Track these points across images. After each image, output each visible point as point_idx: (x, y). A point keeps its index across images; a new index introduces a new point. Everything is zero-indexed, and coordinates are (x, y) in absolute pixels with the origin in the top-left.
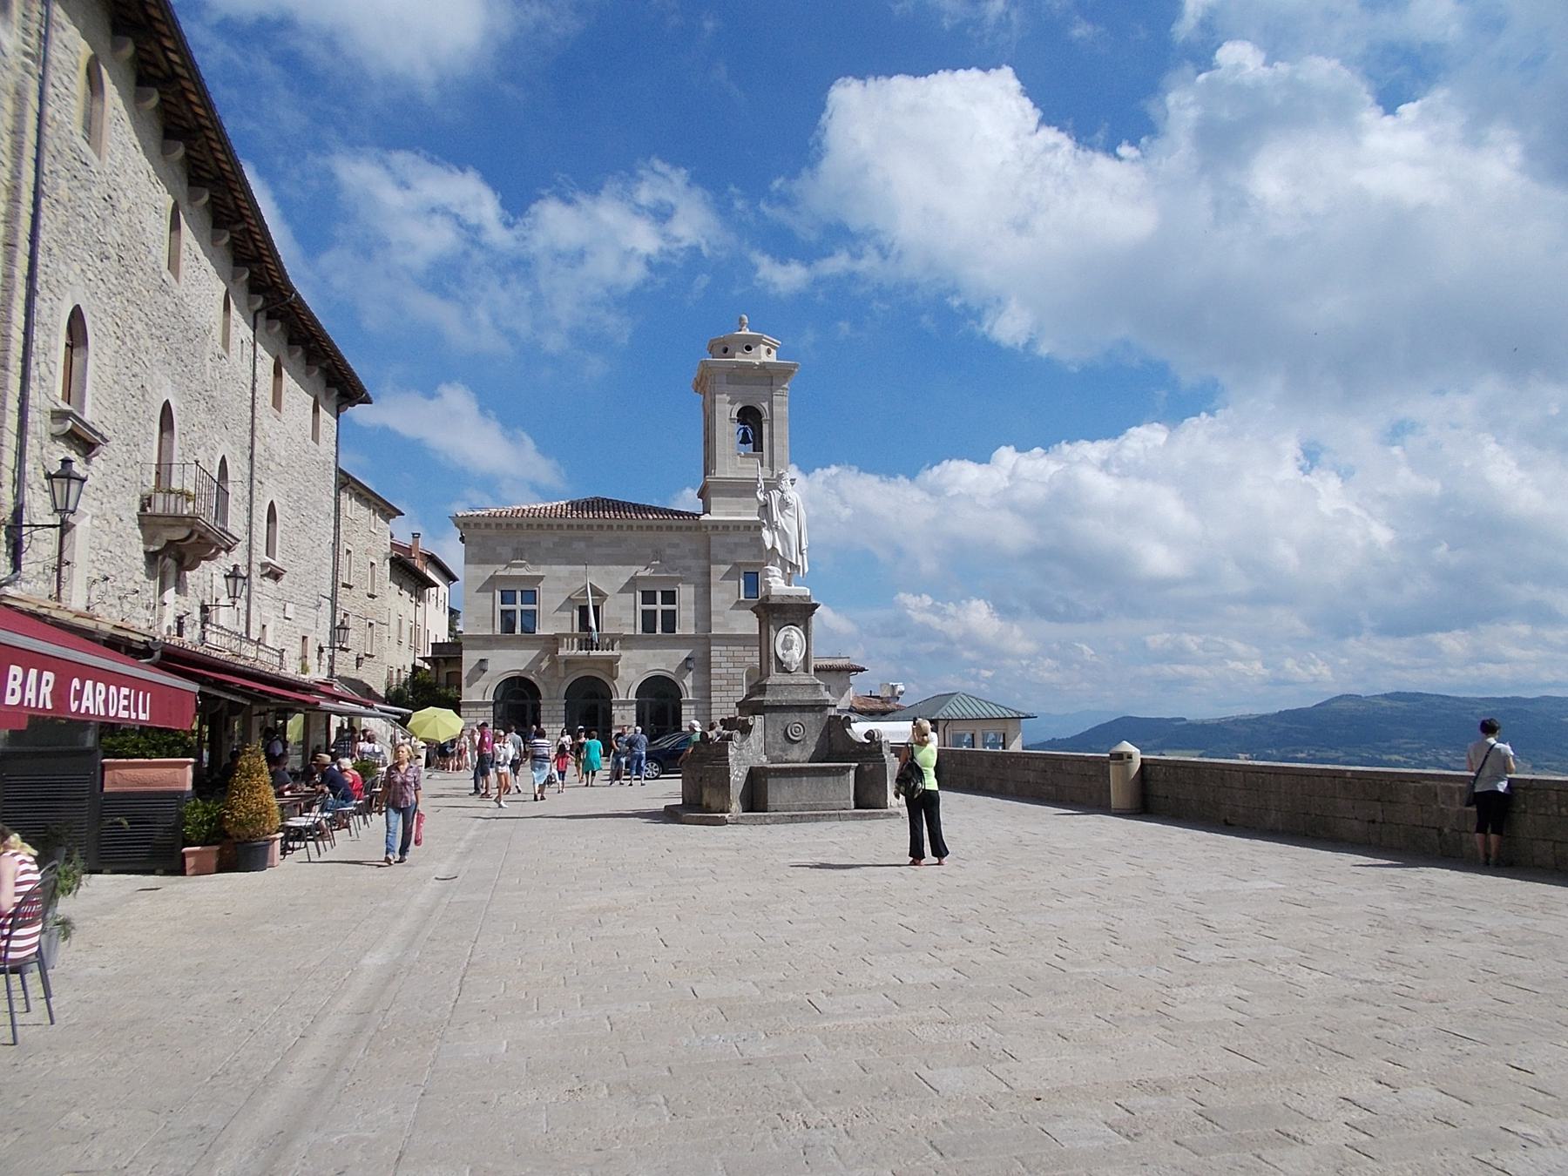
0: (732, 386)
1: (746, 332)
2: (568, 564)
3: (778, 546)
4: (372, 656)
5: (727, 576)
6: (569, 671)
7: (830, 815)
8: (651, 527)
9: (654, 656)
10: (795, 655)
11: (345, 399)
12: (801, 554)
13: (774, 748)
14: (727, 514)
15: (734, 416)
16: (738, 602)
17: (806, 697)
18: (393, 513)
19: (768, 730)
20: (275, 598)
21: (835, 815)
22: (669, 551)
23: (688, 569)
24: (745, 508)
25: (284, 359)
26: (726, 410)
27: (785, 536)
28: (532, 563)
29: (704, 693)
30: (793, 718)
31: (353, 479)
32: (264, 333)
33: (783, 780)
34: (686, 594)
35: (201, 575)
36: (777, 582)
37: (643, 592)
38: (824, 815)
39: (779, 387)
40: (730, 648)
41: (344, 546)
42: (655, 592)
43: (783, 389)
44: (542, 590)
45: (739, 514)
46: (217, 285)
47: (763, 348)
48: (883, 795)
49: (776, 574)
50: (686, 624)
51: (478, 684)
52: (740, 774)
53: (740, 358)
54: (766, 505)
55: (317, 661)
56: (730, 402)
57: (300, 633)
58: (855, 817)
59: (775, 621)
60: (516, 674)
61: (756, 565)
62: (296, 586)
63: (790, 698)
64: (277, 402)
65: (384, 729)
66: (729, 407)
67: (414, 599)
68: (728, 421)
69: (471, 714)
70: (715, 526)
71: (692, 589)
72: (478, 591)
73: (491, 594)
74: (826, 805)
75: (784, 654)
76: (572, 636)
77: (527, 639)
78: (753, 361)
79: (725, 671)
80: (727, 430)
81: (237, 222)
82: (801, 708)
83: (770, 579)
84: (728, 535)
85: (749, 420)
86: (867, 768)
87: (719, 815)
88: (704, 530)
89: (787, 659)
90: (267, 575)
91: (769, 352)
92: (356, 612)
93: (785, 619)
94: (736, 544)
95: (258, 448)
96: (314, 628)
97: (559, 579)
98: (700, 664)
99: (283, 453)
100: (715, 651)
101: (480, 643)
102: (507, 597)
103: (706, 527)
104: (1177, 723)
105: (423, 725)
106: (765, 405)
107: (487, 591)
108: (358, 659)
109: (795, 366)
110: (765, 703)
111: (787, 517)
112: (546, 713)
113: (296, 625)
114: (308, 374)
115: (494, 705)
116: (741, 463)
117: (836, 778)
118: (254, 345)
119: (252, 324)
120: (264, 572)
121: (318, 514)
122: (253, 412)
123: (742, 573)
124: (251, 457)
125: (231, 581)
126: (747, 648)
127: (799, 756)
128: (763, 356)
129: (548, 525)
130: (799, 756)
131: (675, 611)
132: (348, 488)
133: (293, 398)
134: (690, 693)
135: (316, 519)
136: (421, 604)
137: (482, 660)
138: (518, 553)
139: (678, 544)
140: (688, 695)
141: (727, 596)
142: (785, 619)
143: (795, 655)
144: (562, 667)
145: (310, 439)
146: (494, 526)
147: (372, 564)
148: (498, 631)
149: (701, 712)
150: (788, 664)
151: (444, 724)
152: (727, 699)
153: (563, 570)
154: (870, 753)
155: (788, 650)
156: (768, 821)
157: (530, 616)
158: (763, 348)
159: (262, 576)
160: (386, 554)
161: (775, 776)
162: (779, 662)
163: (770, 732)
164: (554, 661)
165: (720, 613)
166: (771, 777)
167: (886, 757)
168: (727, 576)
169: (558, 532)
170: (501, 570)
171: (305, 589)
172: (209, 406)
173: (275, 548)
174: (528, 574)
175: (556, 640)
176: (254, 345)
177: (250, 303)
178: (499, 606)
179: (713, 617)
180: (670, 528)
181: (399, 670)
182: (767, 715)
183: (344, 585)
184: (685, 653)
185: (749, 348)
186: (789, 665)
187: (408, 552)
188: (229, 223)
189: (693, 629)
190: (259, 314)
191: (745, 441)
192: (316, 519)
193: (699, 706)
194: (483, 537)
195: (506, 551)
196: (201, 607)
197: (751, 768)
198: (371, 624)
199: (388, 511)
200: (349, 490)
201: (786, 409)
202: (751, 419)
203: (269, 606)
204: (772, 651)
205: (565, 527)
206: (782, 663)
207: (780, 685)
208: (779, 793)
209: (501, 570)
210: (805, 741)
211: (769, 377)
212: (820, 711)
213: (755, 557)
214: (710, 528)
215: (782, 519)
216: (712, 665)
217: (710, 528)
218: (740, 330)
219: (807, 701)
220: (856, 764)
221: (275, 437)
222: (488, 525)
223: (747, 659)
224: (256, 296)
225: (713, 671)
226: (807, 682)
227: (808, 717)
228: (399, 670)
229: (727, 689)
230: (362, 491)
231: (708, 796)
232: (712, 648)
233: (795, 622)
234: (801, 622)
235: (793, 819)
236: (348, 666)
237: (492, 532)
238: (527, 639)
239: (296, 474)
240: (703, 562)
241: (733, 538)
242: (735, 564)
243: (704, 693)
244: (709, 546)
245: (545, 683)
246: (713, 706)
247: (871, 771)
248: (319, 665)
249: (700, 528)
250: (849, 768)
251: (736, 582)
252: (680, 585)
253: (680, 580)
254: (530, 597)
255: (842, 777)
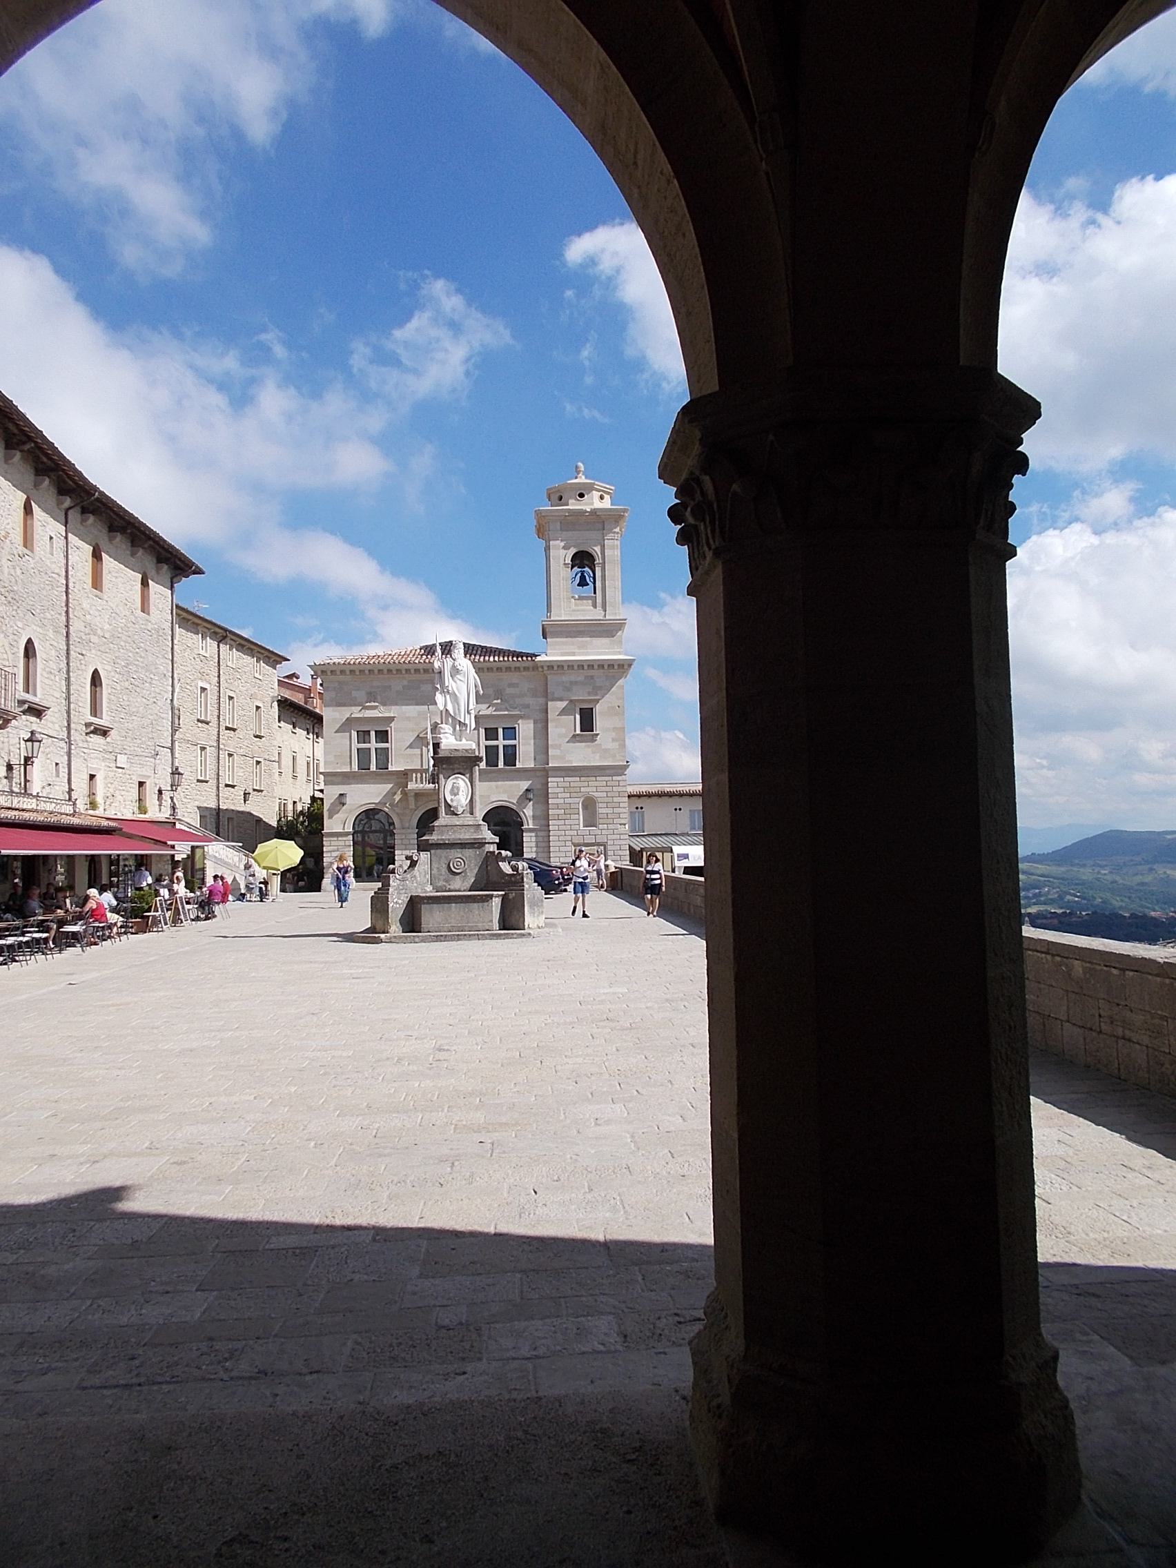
0: (564, 533)
1: (582, 479)
2: (417, 704)
3: (450, 708)
4: (262, 791)
5: (564, 712)
6: (420, 803)
7: (470, 935)
8: (492, 669)
9: (497, 787)
10: (462, 800)
11: (178, 572)
12: (469, 713)
13: (439, 879)
14: (562, 655)
15: (569, 561)
16: (574, 736)
17: (466, 836)
18: (278, 659)
19: (433, 864)
20: (105, 751)
21: (475, 935)
22: (509, 691)
23: (528, 706)
24: (579, 648)
25: (104, 543)
26: (562, 554)
27: (455, 699)
28: (384, 704)
29: (543, 822)
30: (456, 853)
31: (231, 632)
32: (79, 526)
33: (435, 905)
34: (526, 729)
35: (6, 740)
36: (447, 738)
37: (485, 729)
38: (465, 935)
39: (611, 531)
40: (566, 779)
41: (226, 693)
42: (497, 729)
43: (615, 533)
44: (394, 731)
45: (574, 654)
46: (14, 496)
47: (596, 494)
48: (522, 919)
49: (447, 731)
50: (526, 759)
51: (339, 816)
52: (400, 901)
53: (574, 505)
54: (440, 672)
55: (158, 803)
56: (564, 548)
57: (136, 780)
58: (498, 936)
59: (444, 771)
60: (372, 806)
61: (590, 701)
62: (128, 739)
63: (453, 837)
64: (97, 583)
65: (236, 859)
66: (563, 552)
67: (311, 736)
68: (562, 565)
69: (333, 843)
70: (551, 666)
71: (532, 726)
72: (336, 732)
73: (348, 734)
74: (472, 927)
75: (452, 800)
76: (422, 771)
77: (382, 774)
78: (583, 508)
79: (562, 801)
80: (563, 575)
81: (24, 443)
82: (463, 845)
83: (441, 736)
84: (564, 674)
85: (586, 562)
86: (511, 896)
87: (377, 935)
88: (540, 669)
89: (454, 804)
90: (92, 732)
91: (602, 498)
92: (241, 751)
93: (453, 770)
94: (571, 683)
95: (76, 626)
96: (153, 775)
97: (408, 719)
98: (538, 794)
99: (107, 627)
100: (553, 782)
101: (339, 779)
102: (364, 736)
103: (542, 667)
104: (1169, 837)
105: (265, 854)
106: (598, 549)
107: (344, 731)
108: (245, 794)
109: (625, 511)
110: (430, 842)
111: (458, 681)
112: (400, 842)
113: (130, 773)
114: (133, 555)
115: (353, 835)
116: (576, 605)
117: (481, 904)
118: (66, 538)
119: (63, 520)
120: (88, 731)
121: (152, 677)
122: (67, 595)
123: (578, 710)
124: (67, 636)
125: (29, 744)
126: (583, 779)
127: (460, 886)
128: (594, 502)
129: (397, 670)
130: (460, 886)
131: (515, 746)
132: (228, 640)
133: (116, 577)
134: (530, 822)
135: (149, 680)
136: (320, 740)
137: (341, 795)
138: (372, 697)
139: (517, 684)
140: (529, 824)
141: (563, 731)
142: (453, 770)
143: (462, 800)
144: (412, 800)
145: (139, 611)
146: (348, 673)
147: (258, 708)
148: (355, 768)
149: (541, 839)
150: (455, 807)
151: (283, 853)
152: (564, 827)
153: (411, 710)
154: (515, 883)
155: (455, 795)
156: (417, 940)
157: (383, 755)
158: (596, 494)
159: (87, 734)
160: (273, 697)
161: (428, 903)
162: (448, 806)
163: (435, 865)
164: (405, 794)
165: (558, 746)
166: (424, 903)
167: (526, 886)
168: (564, 712)
169: (407, 676)
170: (356, 712)
171: (139, 742)
172: (9, 599)
173: (102, 710)
174: (380, 715)
175: (405, 775)
176: (66, 538)
177: (59, 503)
178: (356, 745)
179: (550, 750)
180: (508, 669)
181: (295, 802)
182: (433, 851)
183: (227, 728)
184: (525, 785)
185: (582, 495)
186: (456, 808)
187: (308, 692)
188: (18, 444)
189: (533, 762)
190: (70, 512)
191: (583, 583)
192: (149, 680)
193: (539, 834)
194: (340, 683)
195: (360, 695)
196: (7, 766)
197: (411, 896)
198: (258, 763)
199: (274, 659)
200: (229, 641)
201: (618, 552)
202: (583, 559)
203: (97, 758)
204: (441, 796)
205: (412, 671)
206: (450, 806)
207: (446, 826)
208: (431, 917)
209: (356, 712)
210: (466, 874)
211: (601, 522)
212: (479, 848)
213: (589, 694)
214: (546, 668)
215: (454, 684)
216: (550, 796)
217: (546, 668)
218: (576, 478)
219: (467, 839)
220: (503, 893)
221: (97, 614)
222: (342, 672)
223: (582, 789)
224: (64, 497)
225: (550, 801)
226: (471, 823)
227: (469, 852)
228: (295, 802)
229: (564, 817)
230: (243, 642)
231: (513, 921)
232: (549, 779)
233: (462, 771)
234: (467, 771)
235: (438, 939)
236: (236, 801)
237: (348, 678)
238: (382, 774)
239: (122, 643)
240: (542, 700)
241: (567, 678)
242: (571, 701)
243: (543, 822)
244: (547, 684)
245: (398, 814)
246: (551, 833)
247: (514, 898)
248: (160, 805)
249: (537, 668)
250: (491, 896)
251: (573, 717)
252: (520, 722)
253: (521, 717)
254: (383, 736)
255: (486, 904)
